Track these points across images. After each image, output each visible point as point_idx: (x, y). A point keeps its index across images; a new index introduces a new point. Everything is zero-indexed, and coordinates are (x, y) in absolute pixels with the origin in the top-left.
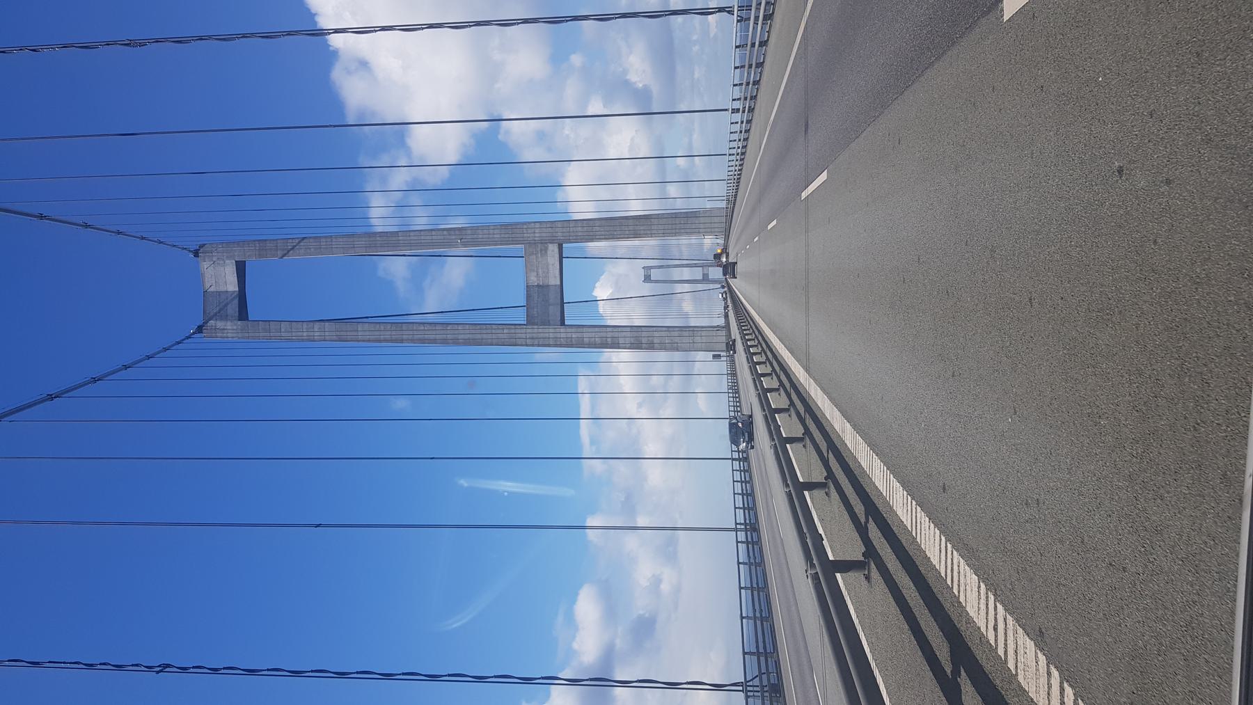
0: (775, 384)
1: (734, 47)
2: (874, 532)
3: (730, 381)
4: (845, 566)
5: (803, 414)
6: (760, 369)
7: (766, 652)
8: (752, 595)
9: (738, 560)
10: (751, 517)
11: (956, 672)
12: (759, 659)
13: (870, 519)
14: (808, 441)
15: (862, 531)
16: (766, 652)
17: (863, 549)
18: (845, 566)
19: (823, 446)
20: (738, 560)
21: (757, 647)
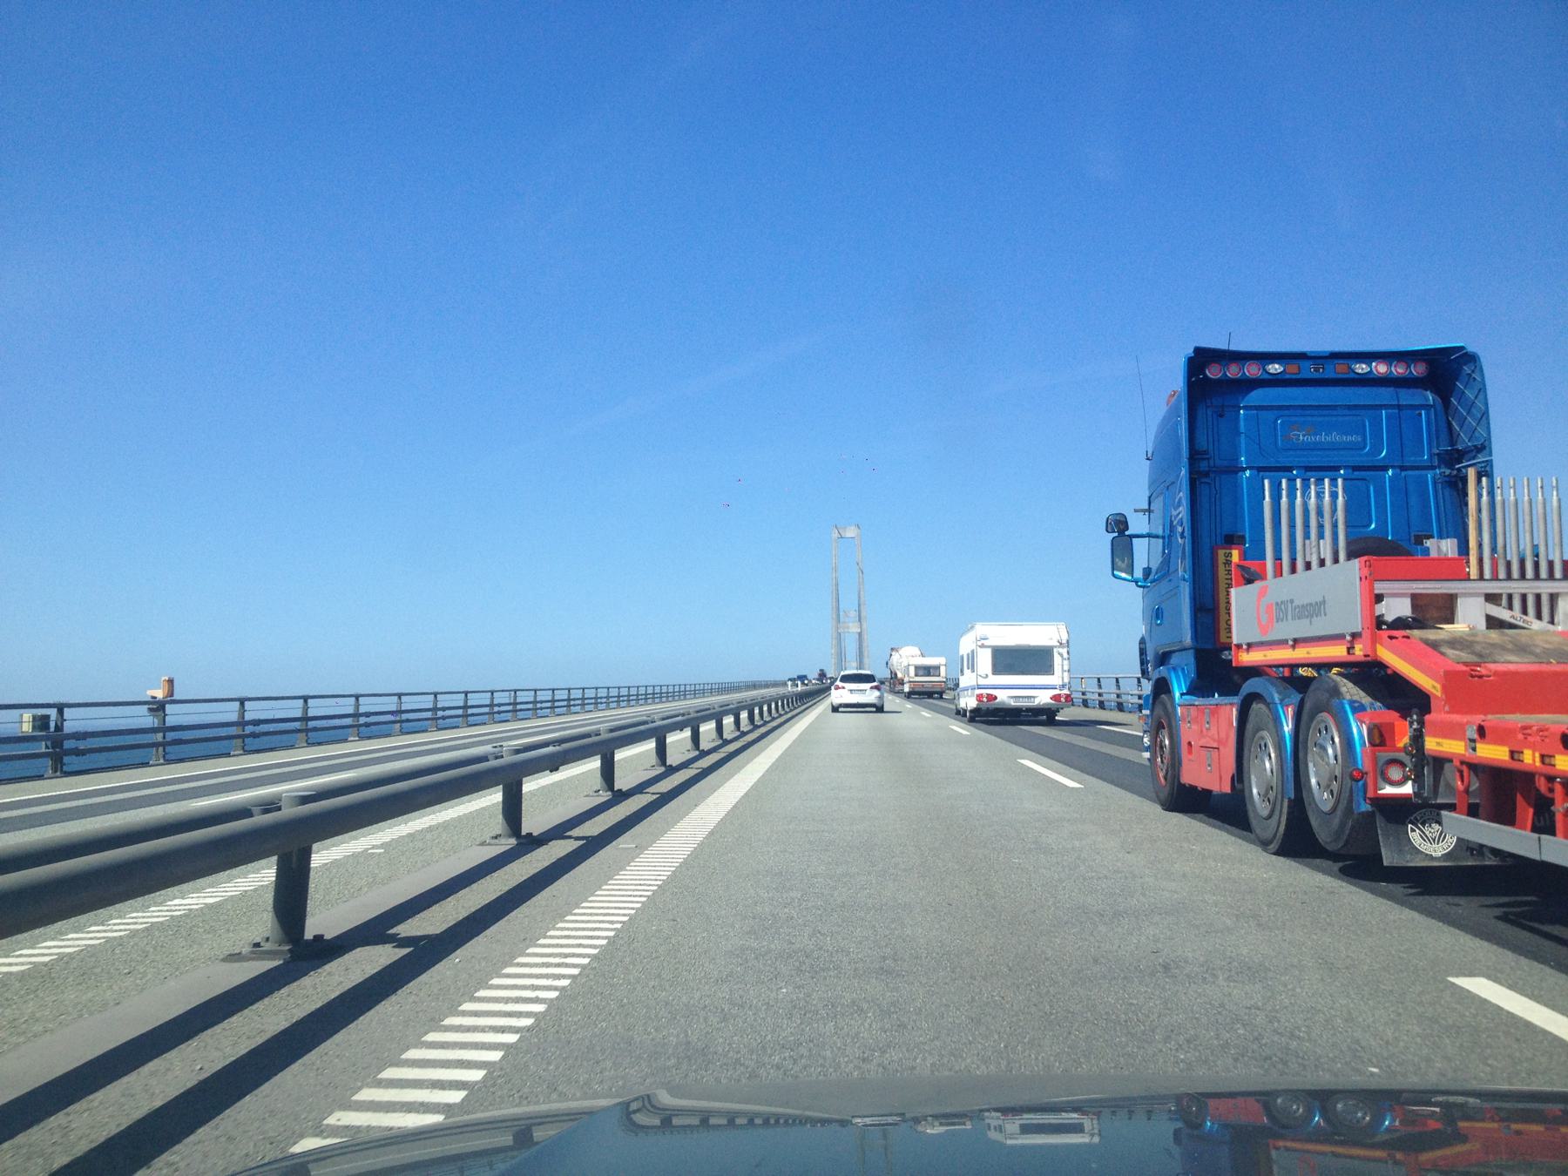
0: (705, 745)
1: (1117, 676)
2: (559, 849)
3: (682, 689)
4: (513, 808)
5: (576, 832)
6: (707, 728)
7: (517, 711)
8: (592, 698)
9: (519, 690)
10: (502, 715)
11: (402, 942)
12: (530, 703)
13: (582, 842)
14: (738, 733)
15: (373, 931)
16: (517, 711)
17: (674, 765)
18: (513, 808)
19: (593, 828)
20: (519, 690)
21: (558, 701)
